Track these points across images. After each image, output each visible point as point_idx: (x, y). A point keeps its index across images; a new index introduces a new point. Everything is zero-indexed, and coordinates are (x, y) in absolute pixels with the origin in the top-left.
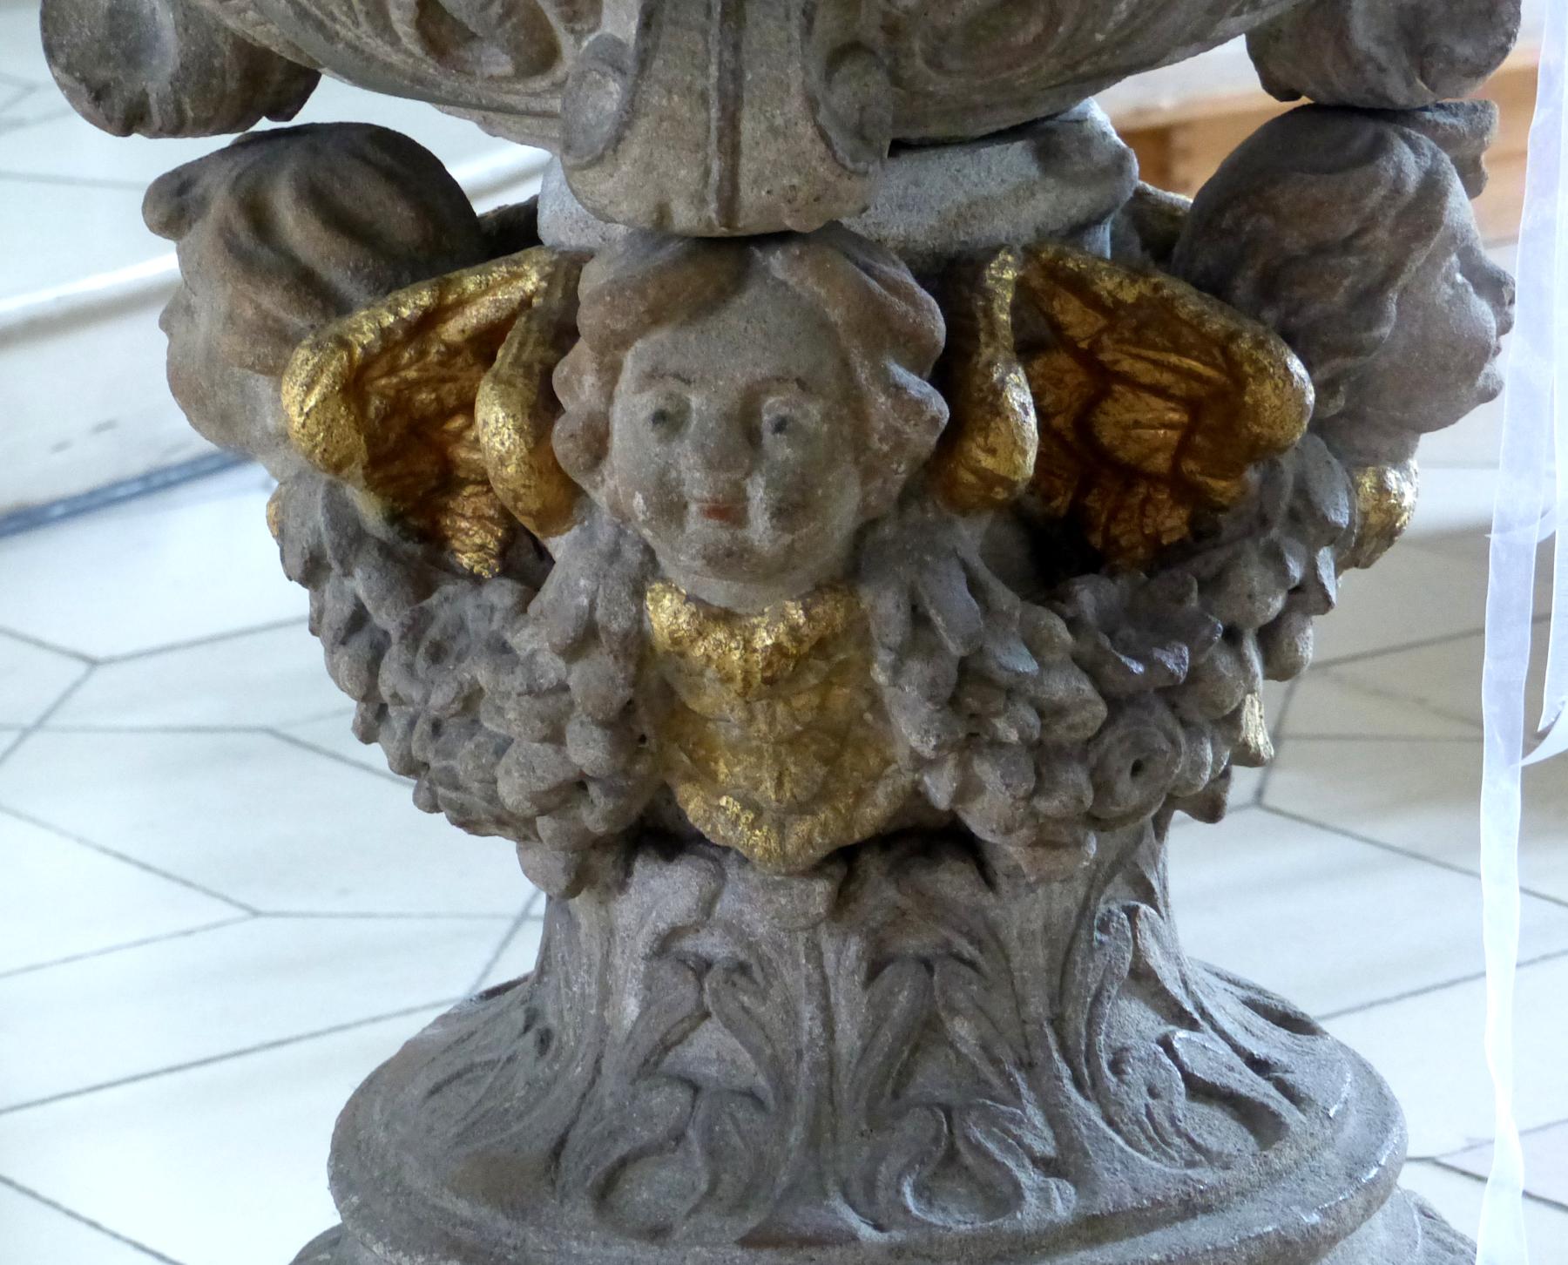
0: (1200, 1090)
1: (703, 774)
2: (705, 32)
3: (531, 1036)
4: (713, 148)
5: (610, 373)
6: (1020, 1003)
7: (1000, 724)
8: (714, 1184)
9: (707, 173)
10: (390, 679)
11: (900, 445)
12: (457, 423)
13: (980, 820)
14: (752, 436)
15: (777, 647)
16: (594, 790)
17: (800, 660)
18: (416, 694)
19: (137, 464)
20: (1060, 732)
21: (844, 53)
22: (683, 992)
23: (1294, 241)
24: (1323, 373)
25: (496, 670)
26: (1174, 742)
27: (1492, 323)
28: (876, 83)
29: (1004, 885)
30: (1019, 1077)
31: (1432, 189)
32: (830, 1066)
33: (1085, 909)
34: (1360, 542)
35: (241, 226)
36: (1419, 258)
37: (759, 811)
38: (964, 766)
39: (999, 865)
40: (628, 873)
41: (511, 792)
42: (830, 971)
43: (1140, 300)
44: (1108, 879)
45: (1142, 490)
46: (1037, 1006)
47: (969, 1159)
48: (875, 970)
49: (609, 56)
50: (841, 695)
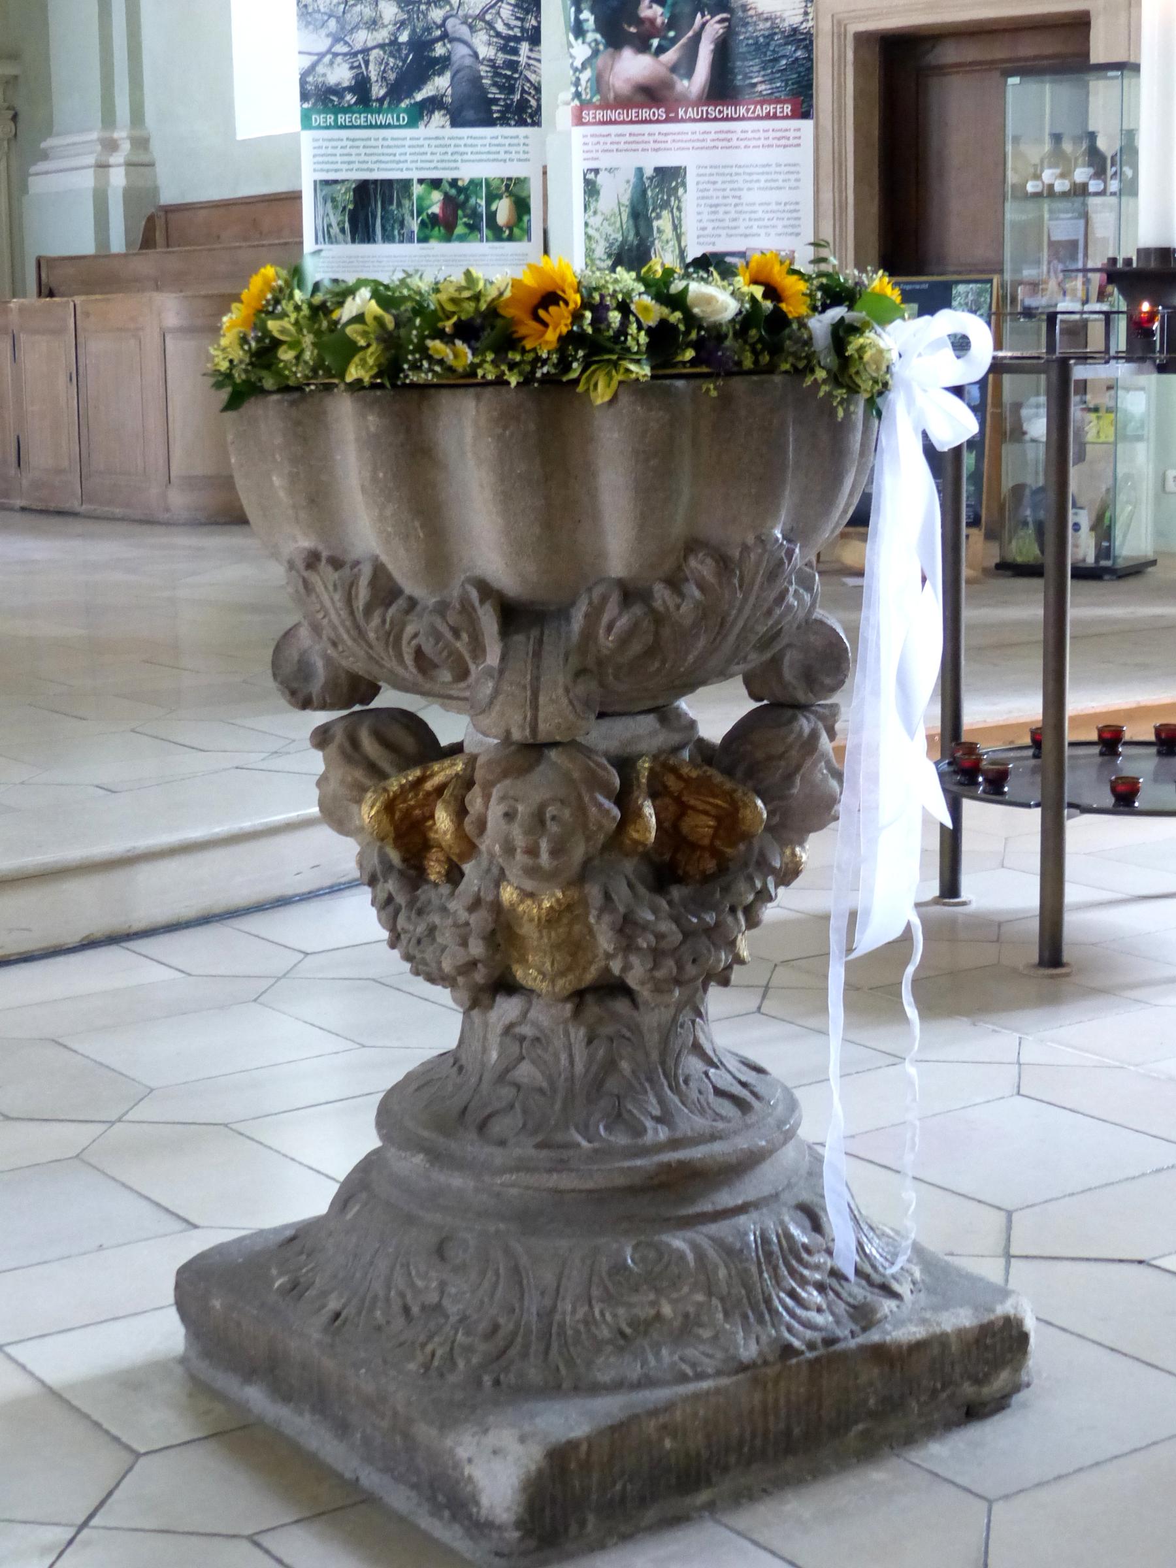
0: (719, 1092)
1: (523, 960)
2: (525, 662)
3: (455, 1068)
4: (528, 708)
5: (487, 797)
6: (647, 1055)
7: (640, 940)
8: (524, 1125)
9: (525, 718)
10: (401, 922)
11: (601, 827)
12: (430, 823)
13: (632, 981)
14: (542, 822)
15: (551, 907)
16: (479, 965)
17: (560, 913)
18: (411, 928)
19: (327, 882)
20: (664, 945)
21: (581, 673)
22: (515, 1049)
23: (760, 755)
24: (771, 807)
25: (442, 918)
26: (709, 951)
27: (838, 790)
28: (593, 685)
29: (642, 1008)
30: (647, 1085)
31: (814, 736)
32: (571, 1079)
33: (674, 1019)
34: (785, 875)
35: (347, 745)
36: (808, 763)
37: (544, 975)
38: (625, 957)
39: (640, 1000)
40: (494, 1000)
41: (447, 966)
42: (573, 1041)
43: (698, 778)
44: (685, 1006)
45: (698, 853)
46: (655, 1056)
47: (626, 1116)
48: (590, 1042)
49: (489, 673)
50: (577, 928)
